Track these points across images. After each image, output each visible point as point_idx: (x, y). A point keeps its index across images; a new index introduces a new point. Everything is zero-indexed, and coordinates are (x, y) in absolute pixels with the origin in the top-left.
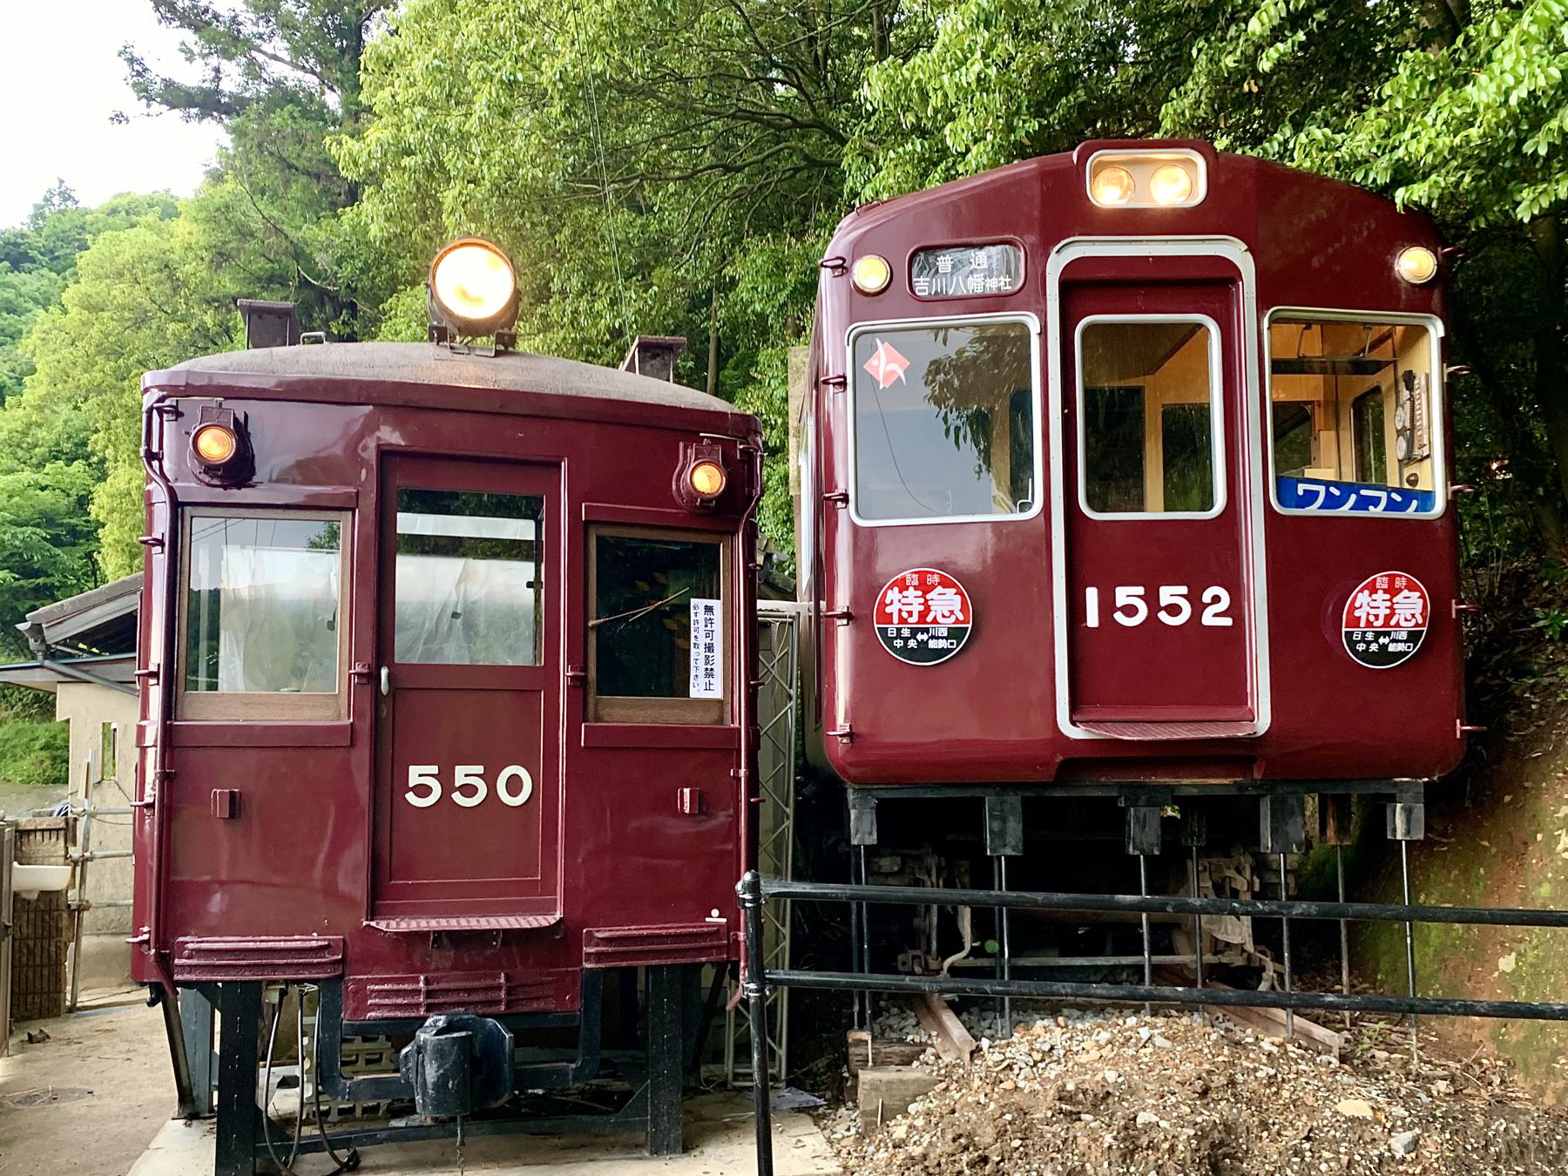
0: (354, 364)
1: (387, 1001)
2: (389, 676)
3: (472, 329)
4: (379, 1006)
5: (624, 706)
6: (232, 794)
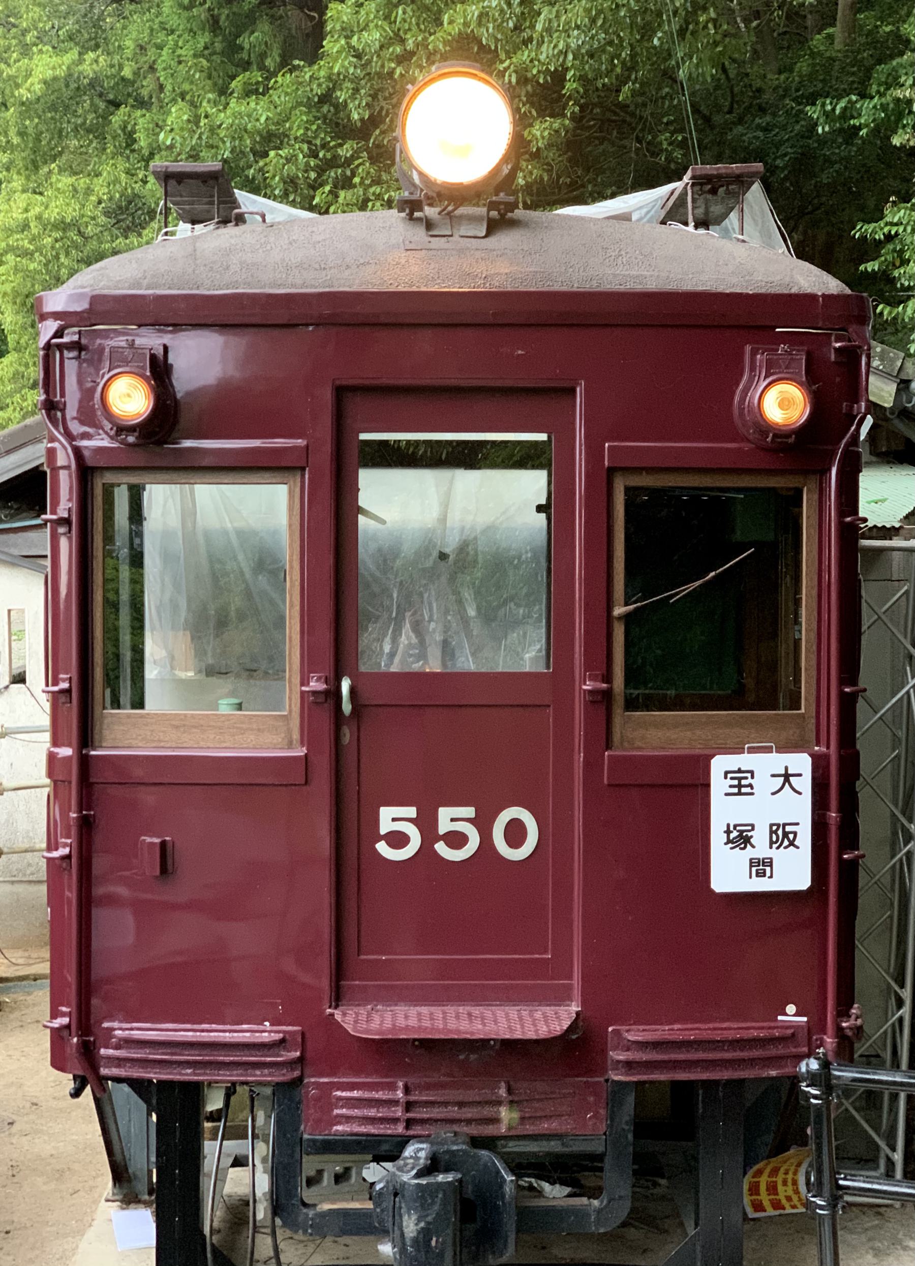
0: (300, 266)
1: (356, 1112)
2: (353, 691)
3: (454, 197)
4: (348, 1119)
6: (163, 844)
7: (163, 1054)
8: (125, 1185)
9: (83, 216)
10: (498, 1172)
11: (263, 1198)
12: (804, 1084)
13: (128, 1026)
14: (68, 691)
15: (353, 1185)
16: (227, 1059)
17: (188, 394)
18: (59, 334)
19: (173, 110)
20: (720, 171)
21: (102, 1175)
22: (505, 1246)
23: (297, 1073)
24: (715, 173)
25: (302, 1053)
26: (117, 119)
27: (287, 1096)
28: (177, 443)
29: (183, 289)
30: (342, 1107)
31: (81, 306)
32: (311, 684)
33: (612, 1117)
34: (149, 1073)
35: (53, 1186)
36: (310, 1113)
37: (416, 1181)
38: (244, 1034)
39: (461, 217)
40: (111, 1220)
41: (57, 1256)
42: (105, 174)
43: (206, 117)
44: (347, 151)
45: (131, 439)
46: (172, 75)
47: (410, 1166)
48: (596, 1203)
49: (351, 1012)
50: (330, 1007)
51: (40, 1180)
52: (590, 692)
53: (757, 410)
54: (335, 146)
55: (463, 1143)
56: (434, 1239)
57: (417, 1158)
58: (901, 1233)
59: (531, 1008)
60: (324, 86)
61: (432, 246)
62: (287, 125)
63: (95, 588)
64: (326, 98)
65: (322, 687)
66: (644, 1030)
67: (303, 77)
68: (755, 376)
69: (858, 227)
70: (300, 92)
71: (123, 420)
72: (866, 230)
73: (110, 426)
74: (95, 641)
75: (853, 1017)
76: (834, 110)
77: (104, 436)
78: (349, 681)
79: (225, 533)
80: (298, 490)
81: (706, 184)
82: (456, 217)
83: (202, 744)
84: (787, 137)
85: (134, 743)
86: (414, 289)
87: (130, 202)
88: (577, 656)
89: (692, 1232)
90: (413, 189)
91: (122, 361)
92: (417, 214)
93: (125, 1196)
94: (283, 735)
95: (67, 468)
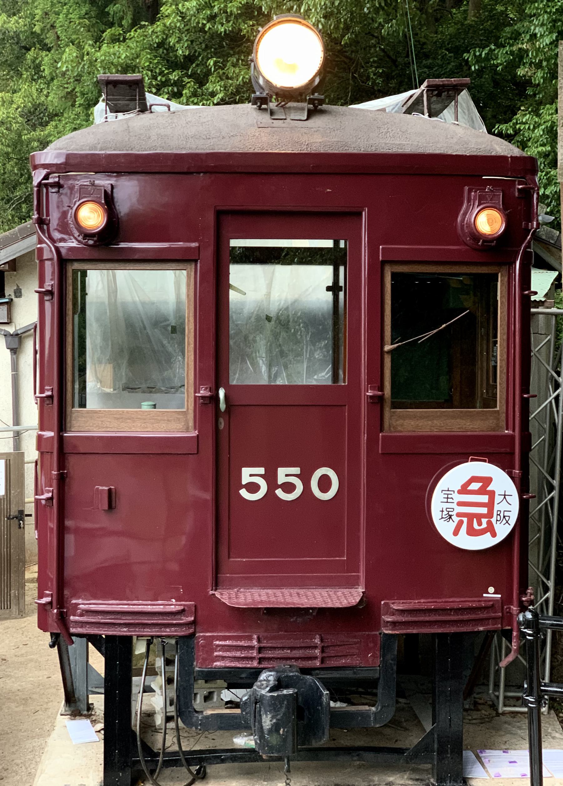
3: (287, 96)
4: (223, 658)
5: (414, 417)
6: (110, 491)
7: (110, 619)
8: (73, 704)
9: (8, 117)
10: (318, 688)
11: (161, 711)
12: (523, 627)
13: (88, 602)
14: (51, 397)
15: (215, 703)
16: (149, 622)
17: (128, 215)
18: (46, 177)
19: (67, 50)
20: (444, 83)
21: (52, 701)
22: (323, 733)
23: (191, 631)
24: (441, 83)
25: (195, 618)
26: (30, 55)
27: (186, 642)
28: (118, 245)
29: (122, 150)
30: (220, 651)
31: (61, 160)
32: (201, 392)
33: (384, 656)
34: (101, 631)
35: (21, 708)
36: (200, 654)
37: (271, 694)
38: (159, 607)
39: (290, 108)
40: (66, 726)
41: (30, 750)
42: (23, 90)
43: (88, 54)
44: (175, 76)
45: (91, 242)
46: (66, 30)
47: (265, 685)
48: (373, 709)
49: (225, 592)
50: (212, 590)
51: (13, 705)
52: (371, 397)
53: (473, 226)
54: (168, 73)
55: (297, 671)
56: (282, 729)
57: (268, 681)
58: (550, 729)
59: (335, 590)
60: (160, 37)
61: (274, 125)
62: (138, 61)
63: (67, 333)
64: (161, 45)
65: (208, 394)
66: (403, 603)
67: (148, 32)
68: (470, 205)
69: (497, 127)
70: (145, 41)
71: (88, 230)
72: (501, 128)
73: (78, 234)
74: (67, 367)
75: (529, 594)
76: (481, 55)
77: (74, 240)
78: (224, 390)
79: (134, 303)
80: (193, 274)
81: (435, 90)
82: (286, 108)
83: (133, 429)
84: (443, 72)
85: (91, 429)
86: (264, 151)
87: (36, 109)
88: (363, 375)
89: (428, 727)
90: (261, 91)
91: (86, 194)
92: (264, 106)
93: (73, 712)
94: (183, 424)
95: (51, 259)
